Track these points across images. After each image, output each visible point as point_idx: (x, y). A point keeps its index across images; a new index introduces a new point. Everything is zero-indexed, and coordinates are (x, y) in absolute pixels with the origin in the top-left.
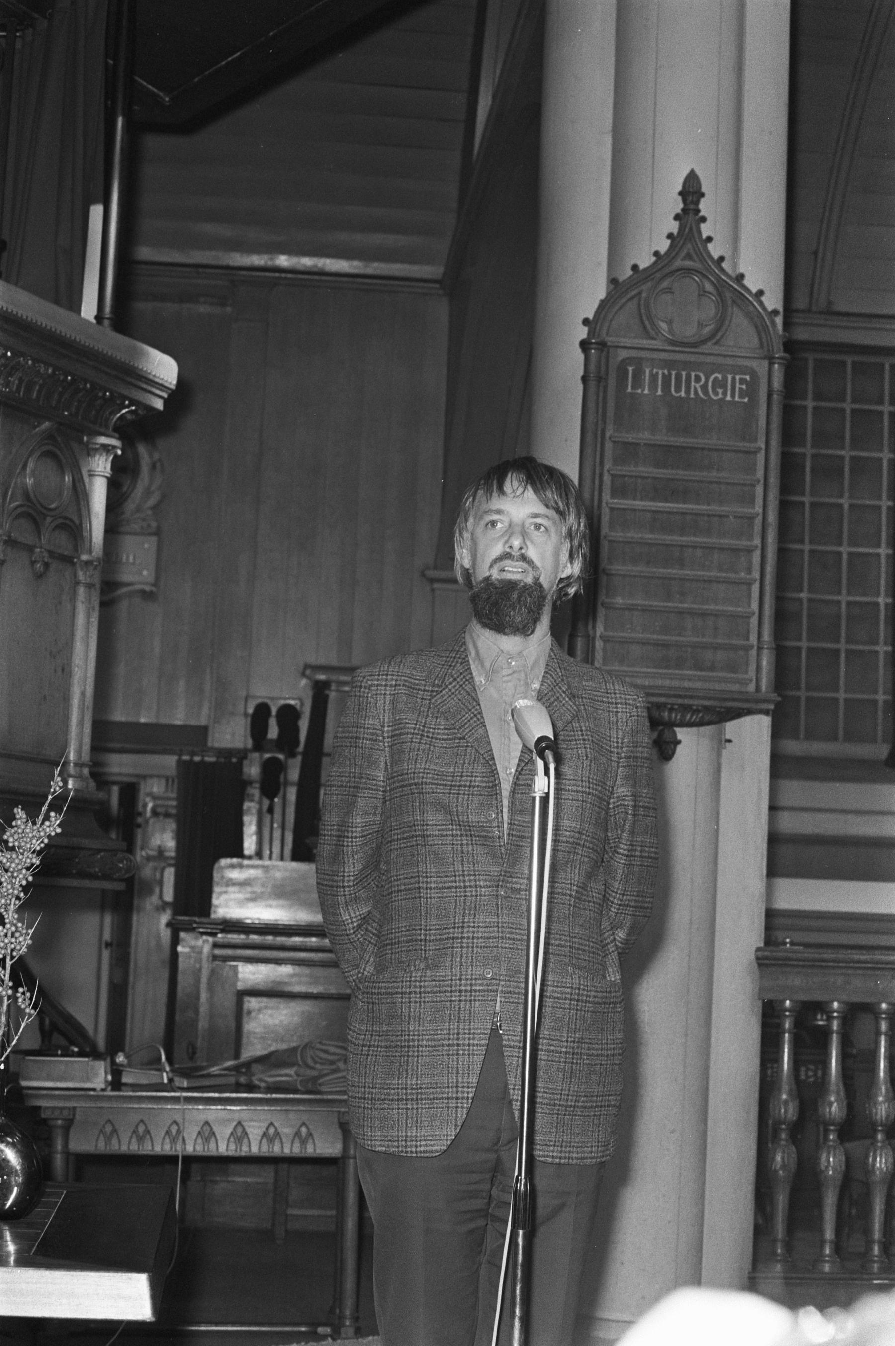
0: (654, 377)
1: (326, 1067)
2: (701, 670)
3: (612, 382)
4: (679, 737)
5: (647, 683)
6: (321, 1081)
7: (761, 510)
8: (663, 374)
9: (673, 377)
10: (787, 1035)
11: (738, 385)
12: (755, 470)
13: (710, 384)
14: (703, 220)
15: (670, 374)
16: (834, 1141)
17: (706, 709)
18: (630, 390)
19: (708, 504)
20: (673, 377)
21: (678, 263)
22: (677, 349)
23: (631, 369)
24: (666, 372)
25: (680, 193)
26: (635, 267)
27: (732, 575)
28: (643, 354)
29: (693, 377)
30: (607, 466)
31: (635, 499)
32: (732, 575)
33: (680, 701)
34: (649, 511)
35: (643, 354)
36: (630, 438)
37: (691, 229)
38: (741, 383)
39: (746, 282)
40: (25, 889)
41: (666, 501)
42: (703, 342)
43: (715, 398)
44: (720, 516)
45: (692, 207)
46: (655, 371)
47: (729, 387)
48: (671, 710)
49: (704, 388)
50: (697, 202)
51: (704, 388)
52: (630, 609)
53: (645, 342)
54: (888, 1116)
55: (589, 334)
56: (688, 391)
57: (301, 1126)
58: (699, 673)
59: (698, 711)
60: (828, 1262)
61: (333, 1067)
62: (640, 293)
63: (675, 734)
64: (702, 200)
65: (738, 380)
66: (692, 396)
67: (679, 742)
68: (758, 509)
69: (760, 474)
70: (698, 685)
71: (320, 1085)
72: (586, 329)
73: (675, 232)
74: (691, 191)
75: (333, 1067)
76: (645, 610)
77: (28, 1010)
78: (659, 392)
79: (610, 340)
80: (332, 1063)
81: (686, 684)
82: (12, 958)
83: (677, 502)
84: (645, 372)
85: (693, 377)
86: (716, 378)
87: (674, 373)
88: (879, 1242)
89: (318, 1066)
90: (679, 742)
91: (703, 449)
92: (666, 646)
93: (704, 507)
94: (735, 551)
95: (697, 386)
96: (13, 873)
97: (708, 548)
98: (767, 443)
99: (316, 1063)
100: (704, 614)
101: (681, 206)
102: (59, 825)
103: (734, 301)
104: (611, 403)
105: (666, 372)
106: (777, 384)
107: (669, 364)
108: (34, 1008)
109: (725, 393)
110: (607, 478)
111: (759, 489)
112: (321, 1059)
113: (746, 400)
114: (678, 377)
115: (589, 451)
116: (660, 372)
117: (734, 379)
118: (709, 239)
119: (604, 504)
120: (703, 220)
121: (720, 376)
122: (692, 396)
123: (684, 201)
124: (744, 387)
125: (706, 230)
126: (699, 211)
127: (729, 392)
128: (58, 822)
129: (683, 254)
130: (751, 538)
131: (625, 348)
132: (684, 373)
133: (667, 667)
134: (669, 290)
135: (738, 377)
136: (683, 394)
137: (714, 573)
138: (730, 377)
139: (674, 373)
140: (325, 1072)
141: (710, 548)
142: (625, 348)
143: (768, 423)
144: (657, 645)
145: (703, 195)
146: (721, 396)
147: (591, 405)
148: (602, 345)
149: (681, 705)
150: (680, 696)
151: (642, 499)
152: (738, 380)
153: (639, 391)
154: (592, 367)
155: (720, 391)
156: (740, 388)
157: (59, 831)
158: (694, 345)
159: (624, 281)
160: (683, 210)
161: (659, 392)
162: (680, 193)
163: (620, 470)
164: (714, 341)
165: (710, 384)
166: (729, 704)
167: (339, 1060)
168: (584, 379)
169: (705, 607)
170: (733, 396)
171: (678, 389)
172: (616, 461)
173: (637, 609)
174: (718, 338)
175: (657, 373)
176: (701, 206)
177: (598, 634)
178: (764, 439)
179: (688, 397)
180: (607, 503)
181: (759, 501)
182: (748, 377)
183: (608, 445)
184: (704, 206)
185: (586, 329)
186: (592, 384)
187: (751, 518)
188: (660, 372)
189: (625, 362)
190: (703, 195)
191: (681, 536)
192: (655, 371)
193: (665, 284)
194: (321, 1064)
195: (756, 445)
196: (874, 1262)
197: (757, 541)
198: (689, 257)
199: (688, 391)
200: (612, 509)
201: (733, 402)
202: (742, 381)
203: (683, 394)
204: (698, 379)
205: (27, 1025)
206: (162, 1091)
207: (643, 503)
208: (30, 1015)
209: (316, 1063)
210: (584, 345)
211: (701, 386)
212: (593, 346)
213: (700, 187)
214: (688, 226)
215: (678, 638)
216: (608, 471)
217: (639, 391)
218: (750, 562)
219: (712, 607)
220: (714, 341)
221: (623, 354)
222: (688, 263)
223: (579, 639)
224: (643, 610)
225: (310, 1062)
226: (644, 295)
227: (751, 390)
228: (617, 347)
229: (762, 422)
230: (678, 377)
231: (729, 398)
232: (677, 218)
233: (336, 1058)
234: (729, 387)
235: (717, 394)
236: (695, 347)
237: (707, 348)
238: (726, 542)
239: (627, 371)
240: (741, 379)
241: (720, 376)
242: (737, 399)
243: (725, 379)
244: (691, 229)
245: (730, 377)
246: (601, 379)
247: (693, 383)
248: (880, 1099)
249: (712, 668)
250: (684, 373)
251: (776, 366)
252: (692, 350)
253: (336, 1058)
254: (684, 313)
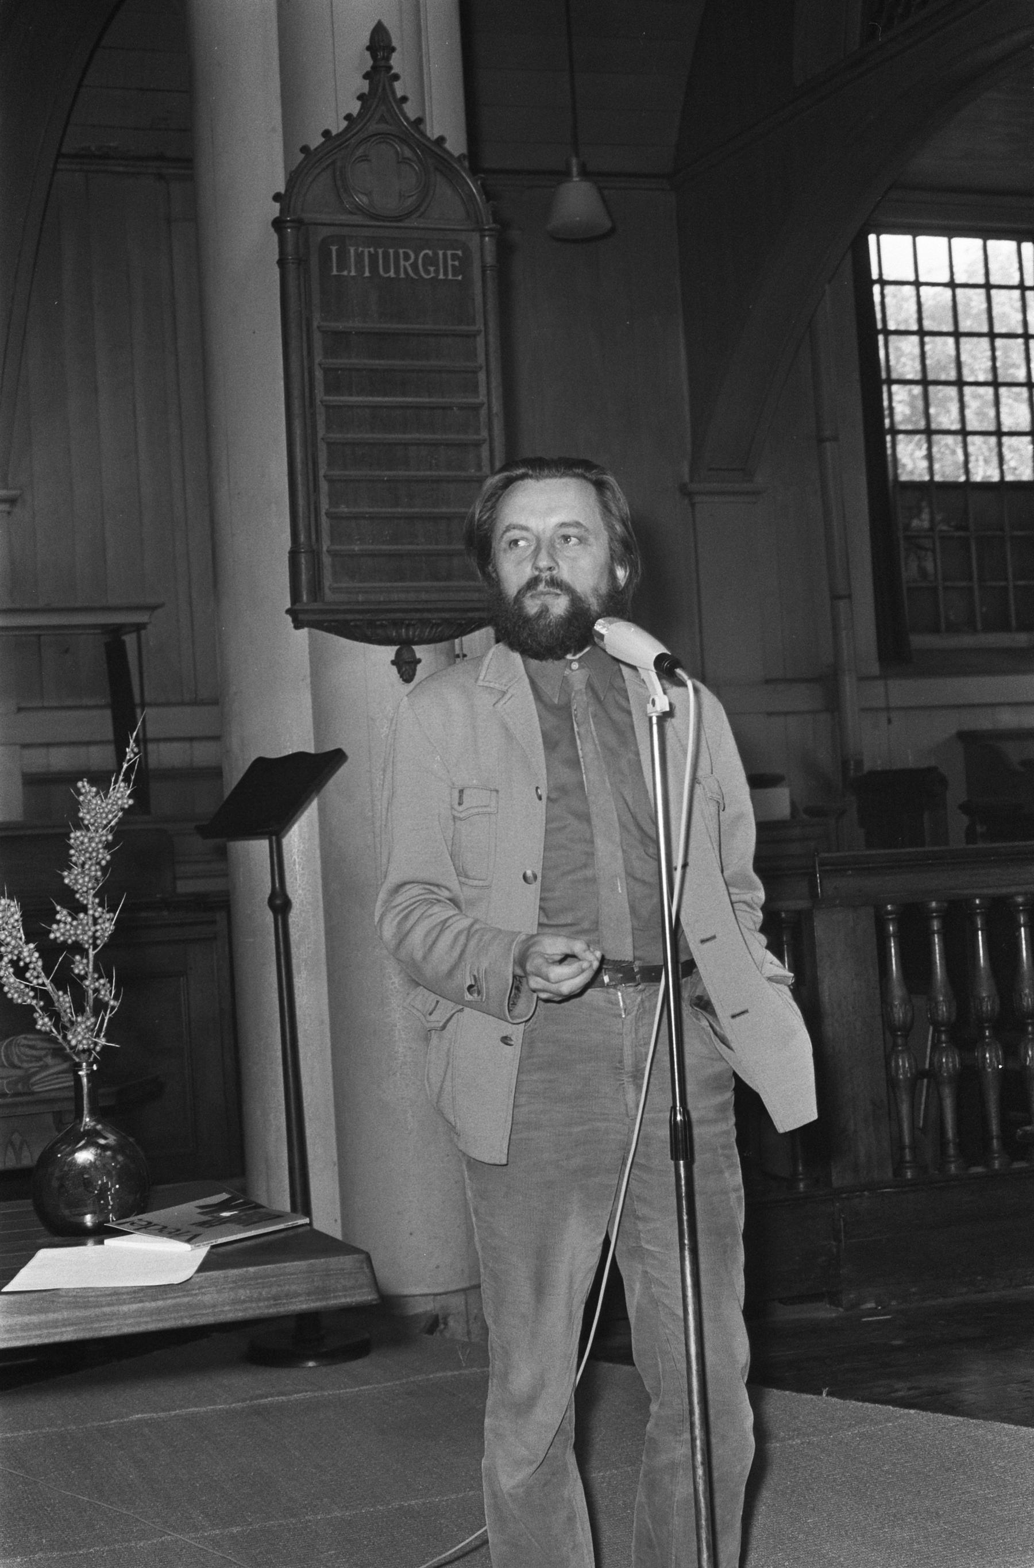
0: (359, 256)
1: (33, 1064)
2: (438, 580)
3: (314, 261)
4: (418, 656)
5: (382, 599)
6: (34, 1079)
7: (485, 400)
8: (369, 252)
9: (380, 256)
10: (1023, 929)
11: (450, 262)
12: (476, 355)
13: (420, 261)
14: (396, 77)
15: (377, 253)
16: (990, 1037)
17: (446, 621)
18: (335, 272)
19: (430, 396)
20: (380, 256)
21: (373, 127)
22: (388, 224)
23: (334, 248)
24: (372, 250)
25: (368, 48)
26: (326, 133)
27: (463, 474)
28: (345, 231)
29: (402, 255)
30: (318, 359)
31: (351, 395)
32: (463, 474)
33: (418, 615)
34: (368, 407)
35: (345, 231)
36: (340, 326)
37: (384, 89)
38: (453, 260)
39: (447, 145)
40: (104, 870)
41: (385, 395)
42: (409, 215)
43: (426, 277)
44: (444, 408)
45: (382, 63)
46: (360, 249)
47: (441, 265)
48: (408, 626)
49: (415, 266)
50: (388, 58)
51: (415, 266)
52: (355, 518)
53: (343, 217)
54: (993, 1009)
55: (282, 211)
56: (397, 272)
57: (13, 1133)
58: (435, 584)
59: (438, 625)
60: (909, 1168)
61: (41, 1063)
62: (333, 163)
63: (413, 651)
64: (394, 55)
65: (449, 257)
66: (402, 275)
67: (419, 661)
68: (482, 398)
69: (481, 359)
70: (434, 596)
71: (33, 1085)
72: (277, 205)
73: (366, 90)
74: (380, 44)
75: (41, 1063)
76: (372, 518)
77: (112, 1003)
78: (367, 274)
79: (307, 216)
80: (39, 1059)
81: (424, 596)
82: (95, 946)
83: (395, 396)
84: (349, 252)
85: (402, 255)
86: (426, 255)
87: (380, 251)
88: (998, 1138)
89: (25, 1065)
90: (419, 661)
91: (418, 335)
92: (399, 555)
93: (427, 400)
94: (462, 445)
95: (407, 264)
96: (91, 853)
97: (434, 445)
98: (486, 324)
99: (22, 1061)
100: (435, 518)
101: (371, 62)
102: (130, 797)
103: (436, 169)
104: (315, 286)
105: (372, 250)
106: (490, 260)
107: (374, 242)
108: (116, 998)
109: (437, 271)
110: (319, 374)
111: (482, 376)
112: (27, 1056)
113: (460, 278)
114: (386, 256)
115: (294, 343)
116: (366, 251)
117: (445, 255)
118: (404, 99)
119: (318, 402)
120: (396, 77)
121: (430, 253)
122: (402, 275)
123: (374, 57)
124: (456, 263)
125: (399, 89)
126: (390, 68)
127: (442, 271)
128: (129, 792)
129: (377, 117)
130: (477, 431)
131: (325, 224)
132: (391, 251)
133: (402, 579)
134: (365, 158)
135: (449, 253)
136: (392, 274)
137: (443, 473)
138: (441, 253)
139: (380, 251)
140: (33, 1070)
141: (435, 444)
142: (325, 224)
143: (485, 303)
144: (391, 555)
145: (393, 49)
146: (432, 275)
147: (292, 290)
148: (299, 223)
149: (420, 620)
150: (417, 610)
151: (358, 395)
152: (449, 257)
153: (345, 273)
154: (290, 248)
155: (432, 269)
156: (453, 265)
157: (131, 802)
158: (398, 219)
159: (316, 149)
160: (373, 67)
161: (367, 274)
162: (368, 48)
163: (332, 362)
164: (418, 214)
165: (420, 261)
166: (470, 615)
167: (46, 1056)
168: (282, 263)
169: (436, 510)
170: (446, 273)
171: (387, 269)
172: (328, 352)
173: (365, 518)
174: (422, 209)
175: (363, 252)
176: (392, 62)
177: (325, 549)
178: (482, 321)
179: (397, 279)
180: (321, 402)
181: (482, 390)
182: (460, 253)
183: (317, 336)
184: (396, 62)
185: (277, 205)
186: (291, 267)
187: (476, 408)
188: (366, 251)
189: (325, 244)
190: (393, 49)
191: (404, 433)
192: (360, 249)
193: (360, 152)
194: (27, 1062)
195: (476, 328)
196: (951, 1162)
197: (485, 434)
198: (382, 119)
199: (397, 272)
200: (328, 407)
201: (446, 280)
202: (454, 257)
203: (392, 274)
204: (407, 257)
205: (110, 1019)
206: (651, 1034)
207: (360, 399)
208: (113, 1008)
209: (22, 1061)
210: (278, 224)
211: (411, 265)
212: (288, 224)
213: (390, 41)
214: (381, 84)
215: (410, 547)
216: (320, 365)
217: (345, 273)
218: (479, 457)
219: (444, 510)
220: (418, 214)
221: (325, 232)
222: (383, 127)
223: (303, 555)
224: (371, 518)
225: (16, 1061)
226: (339, 164)
227: (464, 265)
228: (315, 224)
229: (479, 299)
230: (386, 256)
231: (441, 277)
232: (366, 76)
233: (43, 1053)
234: (441, 265)
235: (428, 272)
236: (400, 221)
237: (413, 222)
238: (452, 436)
239: (331, 251)
240: (452, 255)
241: (430, 253)
242: (450, 277)
243: (436, 254)
244: (384, 89)
245: (441, 253)
246: (302, 262)
247: (402, 263)
248: (1027, 991)
249: (449, 577)
250: (391, 251)
251: (487, 239)
252: (395, 224)
253: (43, 1053)
254: (381, 183)
